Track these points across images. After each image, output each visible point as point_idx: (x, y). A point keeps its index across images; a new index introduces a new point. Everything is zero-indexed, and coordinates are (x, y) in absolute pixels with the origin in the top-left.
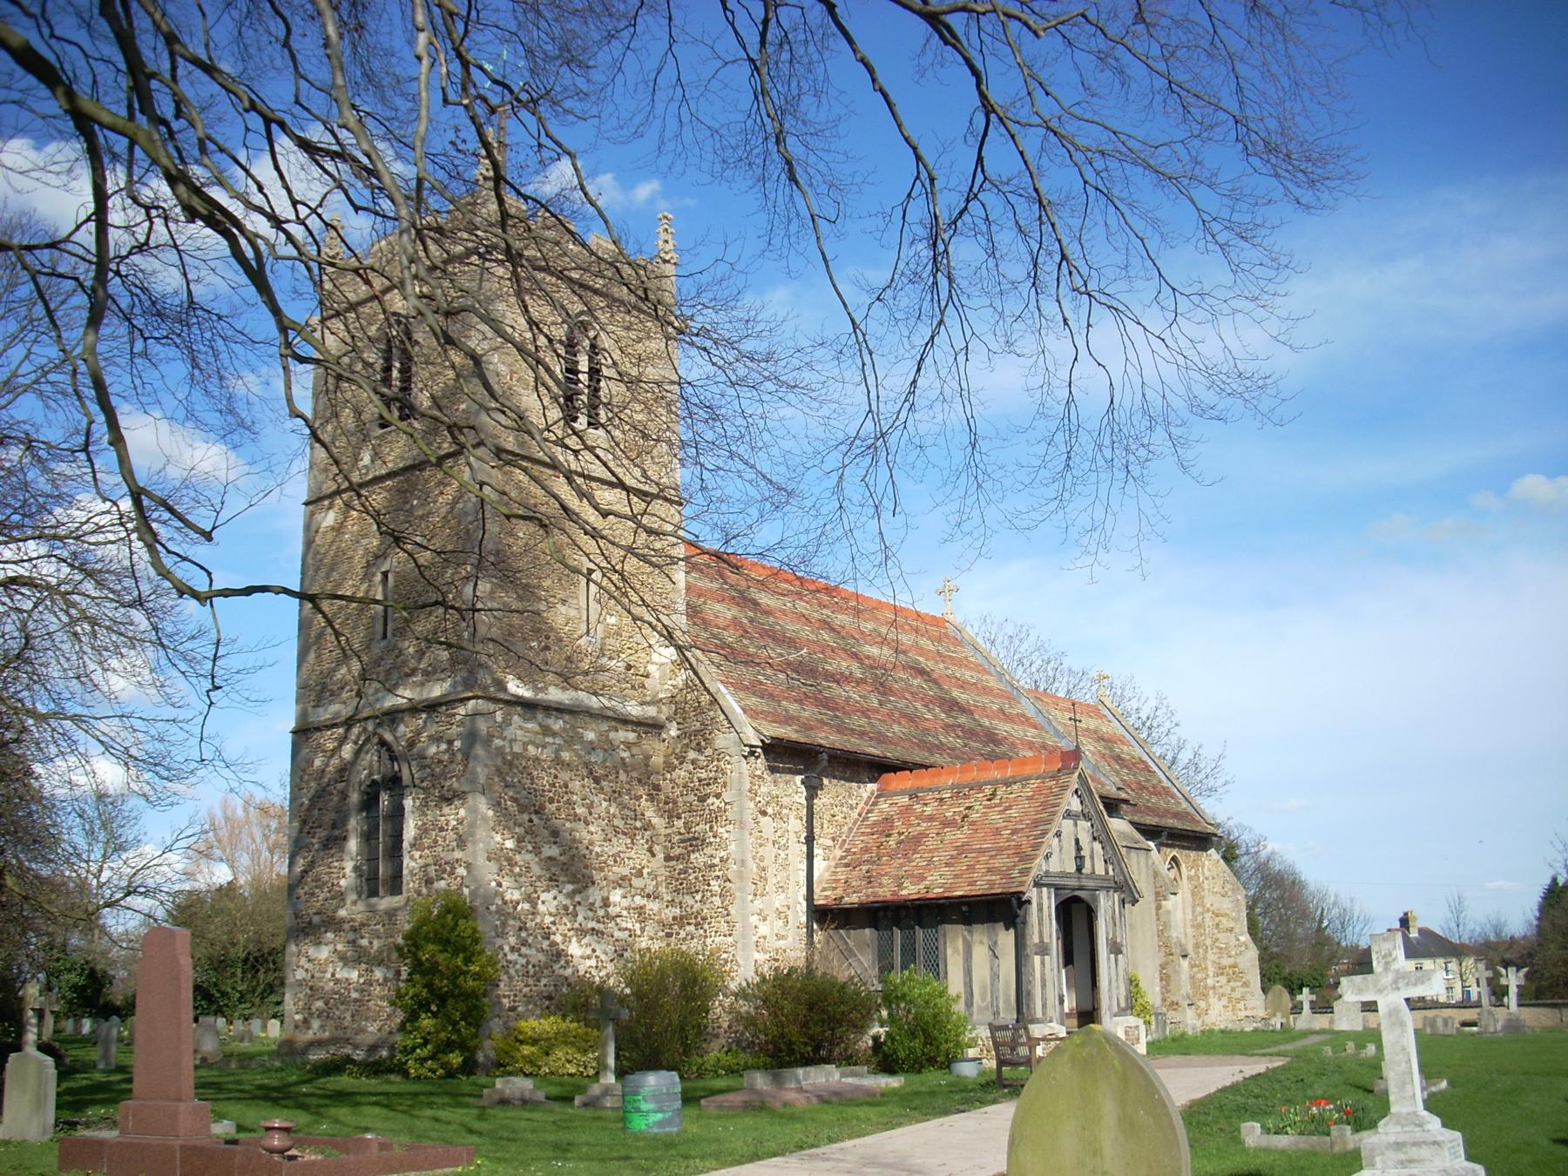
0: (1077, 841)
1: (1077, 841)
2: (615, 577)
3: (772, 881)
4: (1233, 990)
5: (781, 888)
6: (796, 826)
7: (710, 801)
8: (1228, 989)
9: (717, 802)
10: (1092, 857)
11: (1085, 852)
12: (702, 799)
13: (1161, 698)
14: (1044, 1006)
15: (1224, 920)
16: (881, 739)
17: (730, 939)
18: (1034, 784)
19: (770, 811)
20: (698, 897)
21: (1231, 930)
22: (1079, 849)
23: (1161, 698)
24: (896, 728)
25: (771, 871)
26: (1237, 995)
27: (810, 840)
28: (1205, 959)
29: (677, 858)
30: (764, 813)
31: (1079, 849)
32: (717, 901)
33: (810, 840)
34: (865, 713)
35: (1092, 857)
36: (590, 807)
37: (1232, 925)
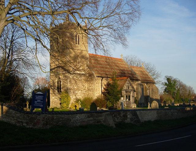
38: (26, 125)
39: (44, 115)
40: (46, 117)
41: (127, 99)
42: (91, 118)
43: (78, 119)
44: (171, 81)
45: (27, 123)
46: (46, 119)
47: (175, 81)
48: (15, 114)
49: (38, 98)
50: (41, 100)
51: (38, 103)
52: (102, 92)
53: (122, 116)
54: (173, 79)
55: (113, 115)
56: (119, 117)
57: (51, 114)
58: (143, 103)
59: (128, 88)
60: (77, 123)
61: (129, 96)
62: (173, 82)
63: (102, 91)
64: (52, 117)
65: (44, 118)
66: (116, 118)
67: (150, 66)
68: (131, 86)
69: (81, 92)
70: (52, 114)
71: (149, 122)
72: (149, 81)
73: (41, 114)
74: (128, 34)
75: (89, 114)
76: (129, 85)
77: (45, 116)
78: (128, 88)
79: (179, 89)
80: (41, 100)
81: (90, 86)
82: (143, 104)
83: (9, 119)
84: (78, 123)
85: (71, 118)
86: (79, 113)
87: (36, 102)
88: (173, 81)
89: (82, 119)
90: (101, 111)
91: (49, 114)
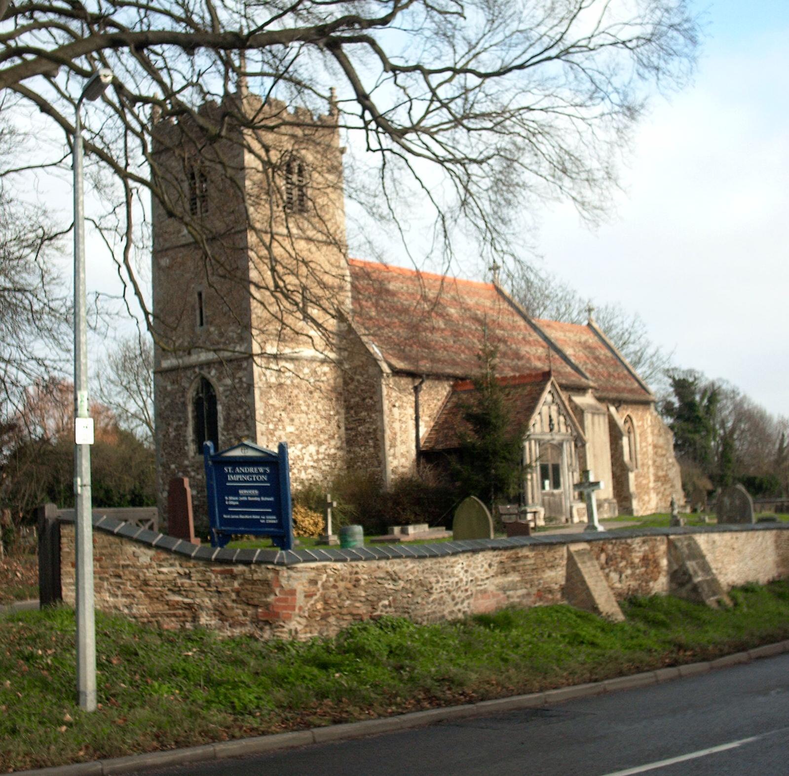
0: (550, 416)
1: (550, 416)
2: (295, 192)
3: (399, 439)
4: (665, 489)
5: (403, 442)
6: (411, 411)
7: (367, 400)
8: (662, 489)
9: (371, 401)
10: (559, 424)
11: (555, 422)
12: (364, 399)
13: (637, 316)
14: (533, 498)
15: (660, 450)
16: (454, 363)
17: (379, 469)
18: (529, 388)
19: (397, 404)
20: (363, 448)
21: (664, 455)
22: (551, 420)
23: (637, 316)
24: (463, 356)
25: (399, 435)
26: (667, 492)
27: (417, 419)
28: (648, 472)
29: (351, 429)
30: (394, 406)
31: (551, 420)
32: (372, 450)
33: (417, 419)
34: (445, 348)
35: (559, 424)
36: (308, 406)
37: (664, 452)
38: (214, 622)
39: (313, 565)
40: (324, 576)
41: (547, 482)
42: (514, 577)
43: (461, 580)
44: (693, 393)
45: (220, 613)
46: (323, 585)
47: (713, 395)
48: (154, 564)
49: (247, 478)
50: (263, 491)
51: (243, 504)
52: (417, 446)
53: (637, 560)
54: (702, 384)
55: (603, 557)
56: (626, 567)
57: (344, 560)
58: (606, 500)
59: (551, 430)
60: (456, 604)
61: (556, 469)
62: (702, 399)
63: (422, 443)
64: (351, 573)
65: (313, 582)
66: (615, 570)
67: (615, 322)
68: (562, 419)
69: (318, 452)
70: (352, 560)
71: (748, 589)
72: (624, 390)
73: (298, 562)
74: (626, 149)
75: (507, 553)
76: (554, 415)
77: (317, 569)
78: (551, 430)
79: (733, 431)
80: (263, 491)
81: (362, 421)
82: (606, 505)
83: (115, 596)
84: (462, 602)
85: (433, 579)
86: (464, 552)
87: (231, 500)
88: (704, 393)
89: (476, 579)
90: (607, 536)
91: (336, 561)
